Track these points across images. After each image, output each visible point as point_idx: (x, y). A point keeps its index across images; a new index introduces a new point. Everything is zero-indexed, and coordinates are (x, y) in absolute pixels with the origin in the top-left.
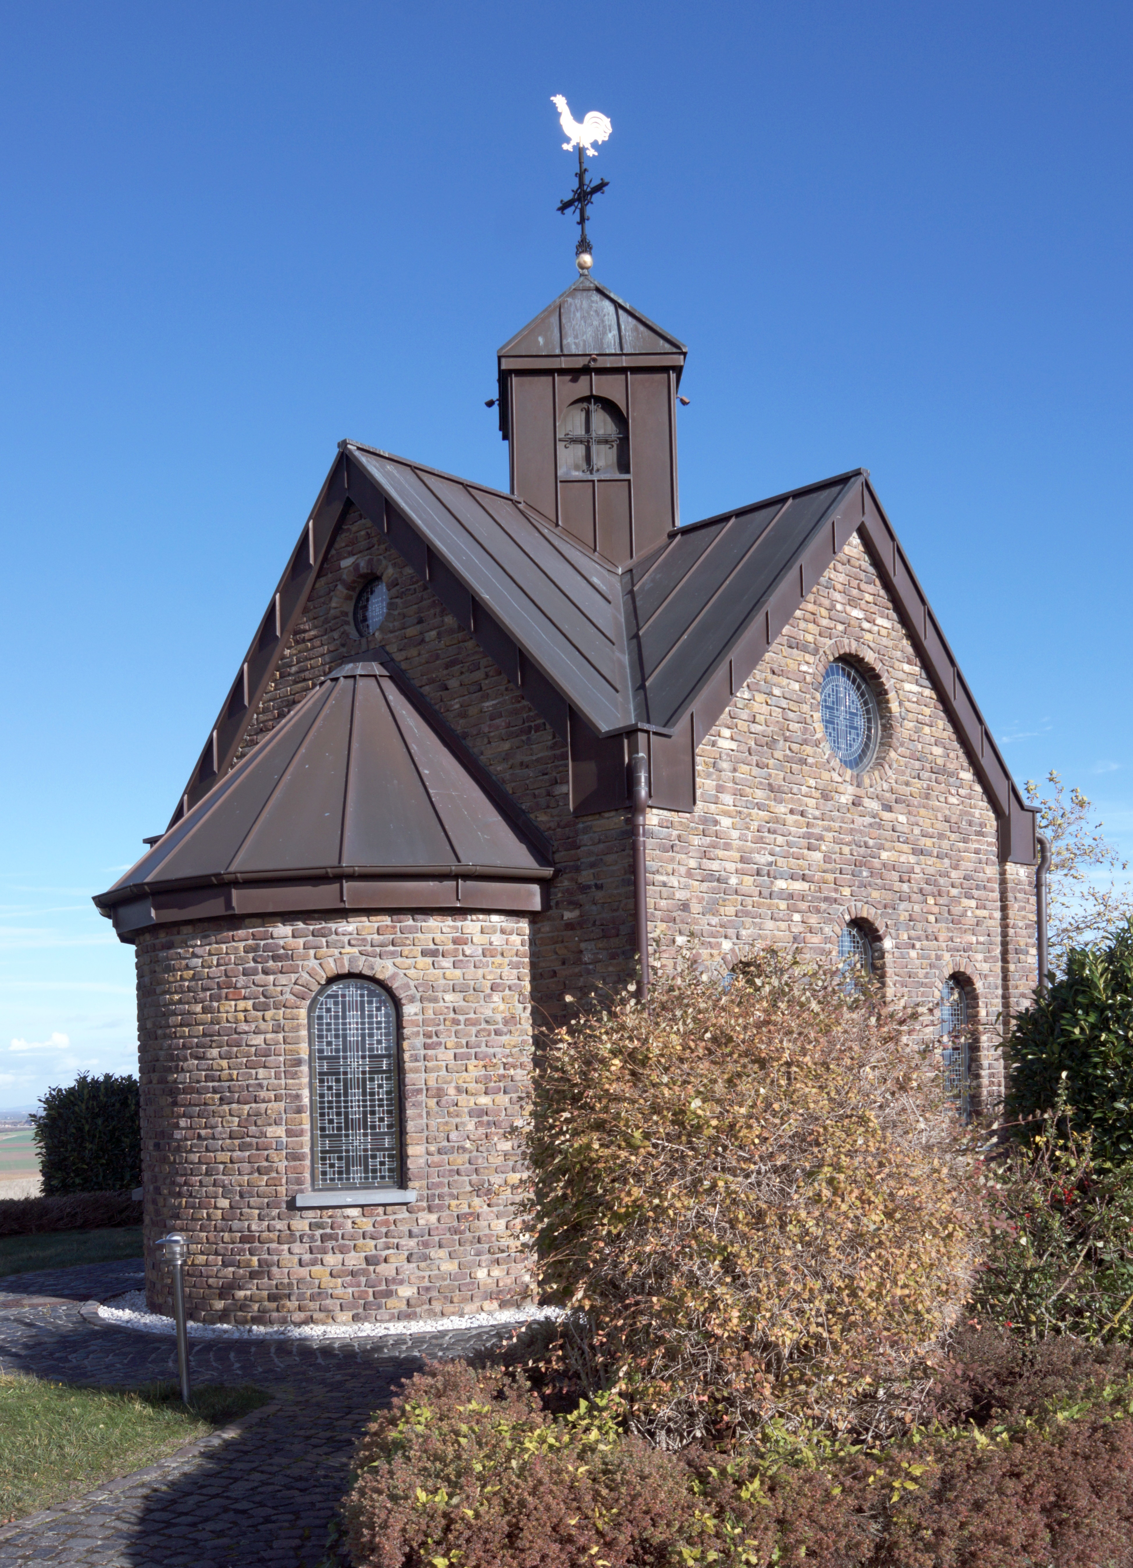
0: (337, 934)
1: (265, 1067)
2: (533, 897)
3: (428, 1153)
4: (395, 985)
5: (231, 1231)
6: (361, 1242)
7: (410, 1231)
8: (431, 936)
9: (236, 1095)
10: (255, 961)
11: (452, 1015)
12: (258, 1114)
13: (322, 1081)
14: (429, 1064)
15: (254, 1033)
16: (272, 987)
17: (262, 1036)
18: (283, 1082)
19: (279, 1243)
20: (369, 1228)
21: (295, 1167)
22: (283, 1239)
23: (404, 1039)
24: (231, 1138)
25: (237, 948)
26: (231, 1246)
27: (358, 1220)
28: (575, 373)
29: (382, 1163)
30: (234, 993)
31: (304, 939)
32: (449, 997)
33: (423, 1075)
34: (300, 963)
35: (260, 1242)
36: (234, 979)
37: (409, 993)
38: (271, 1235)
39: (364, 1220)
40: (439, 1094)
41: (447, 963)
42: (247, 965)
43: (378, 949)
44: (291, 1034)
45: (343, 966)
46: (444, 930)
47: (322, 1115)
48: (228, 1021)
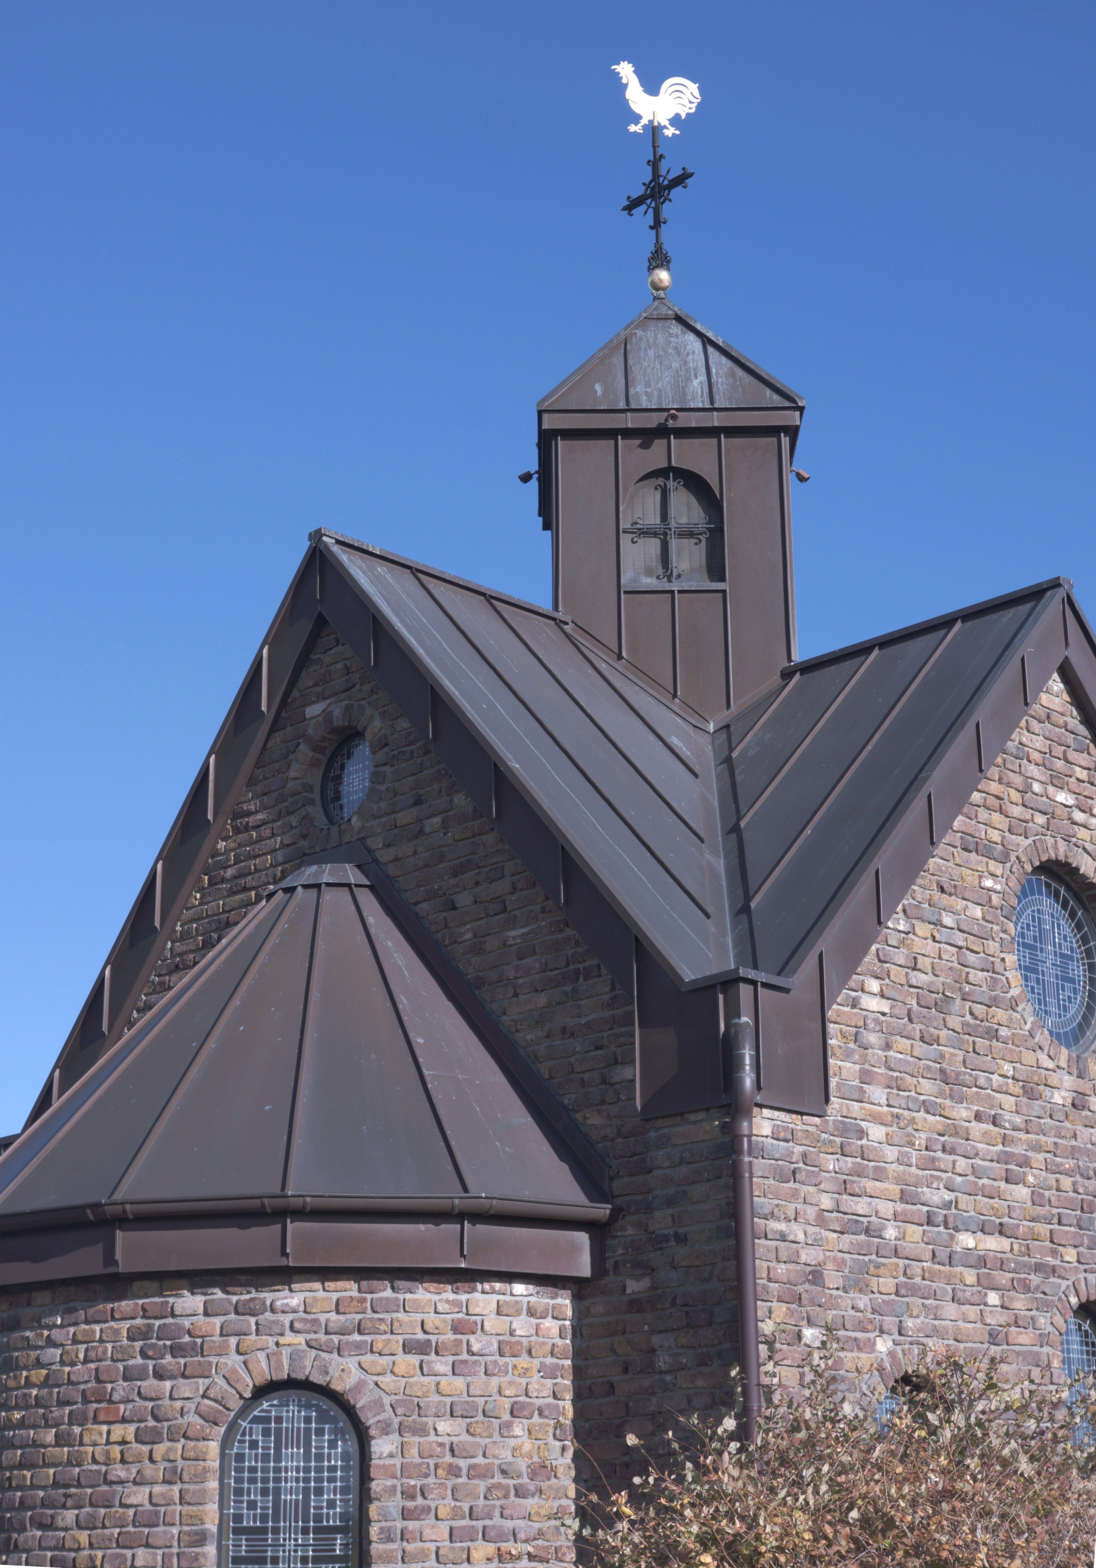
0: (273, 1310)
2: (578, 1254)
4: (360, 1402)
8: (419, 1317)
10: (144, 1355)
11: (448, 1459)
14: (410, 1547)
15: (135, 1483)
16: (167, 1402)
17: (147, 1490)
23: (370, 1500)
25: (117, 1332)
28: (646, 436)
31: (222, 1319)
32: (444, 1426)
36: (109, 1386)
37: (381, 1417)
41: (442, 1365)
42: (131, 1362)
43: (335, 1339)
44: (192, 1487)
45: (280, 1366)
46: (440, 1308)
48: (94, 1461)
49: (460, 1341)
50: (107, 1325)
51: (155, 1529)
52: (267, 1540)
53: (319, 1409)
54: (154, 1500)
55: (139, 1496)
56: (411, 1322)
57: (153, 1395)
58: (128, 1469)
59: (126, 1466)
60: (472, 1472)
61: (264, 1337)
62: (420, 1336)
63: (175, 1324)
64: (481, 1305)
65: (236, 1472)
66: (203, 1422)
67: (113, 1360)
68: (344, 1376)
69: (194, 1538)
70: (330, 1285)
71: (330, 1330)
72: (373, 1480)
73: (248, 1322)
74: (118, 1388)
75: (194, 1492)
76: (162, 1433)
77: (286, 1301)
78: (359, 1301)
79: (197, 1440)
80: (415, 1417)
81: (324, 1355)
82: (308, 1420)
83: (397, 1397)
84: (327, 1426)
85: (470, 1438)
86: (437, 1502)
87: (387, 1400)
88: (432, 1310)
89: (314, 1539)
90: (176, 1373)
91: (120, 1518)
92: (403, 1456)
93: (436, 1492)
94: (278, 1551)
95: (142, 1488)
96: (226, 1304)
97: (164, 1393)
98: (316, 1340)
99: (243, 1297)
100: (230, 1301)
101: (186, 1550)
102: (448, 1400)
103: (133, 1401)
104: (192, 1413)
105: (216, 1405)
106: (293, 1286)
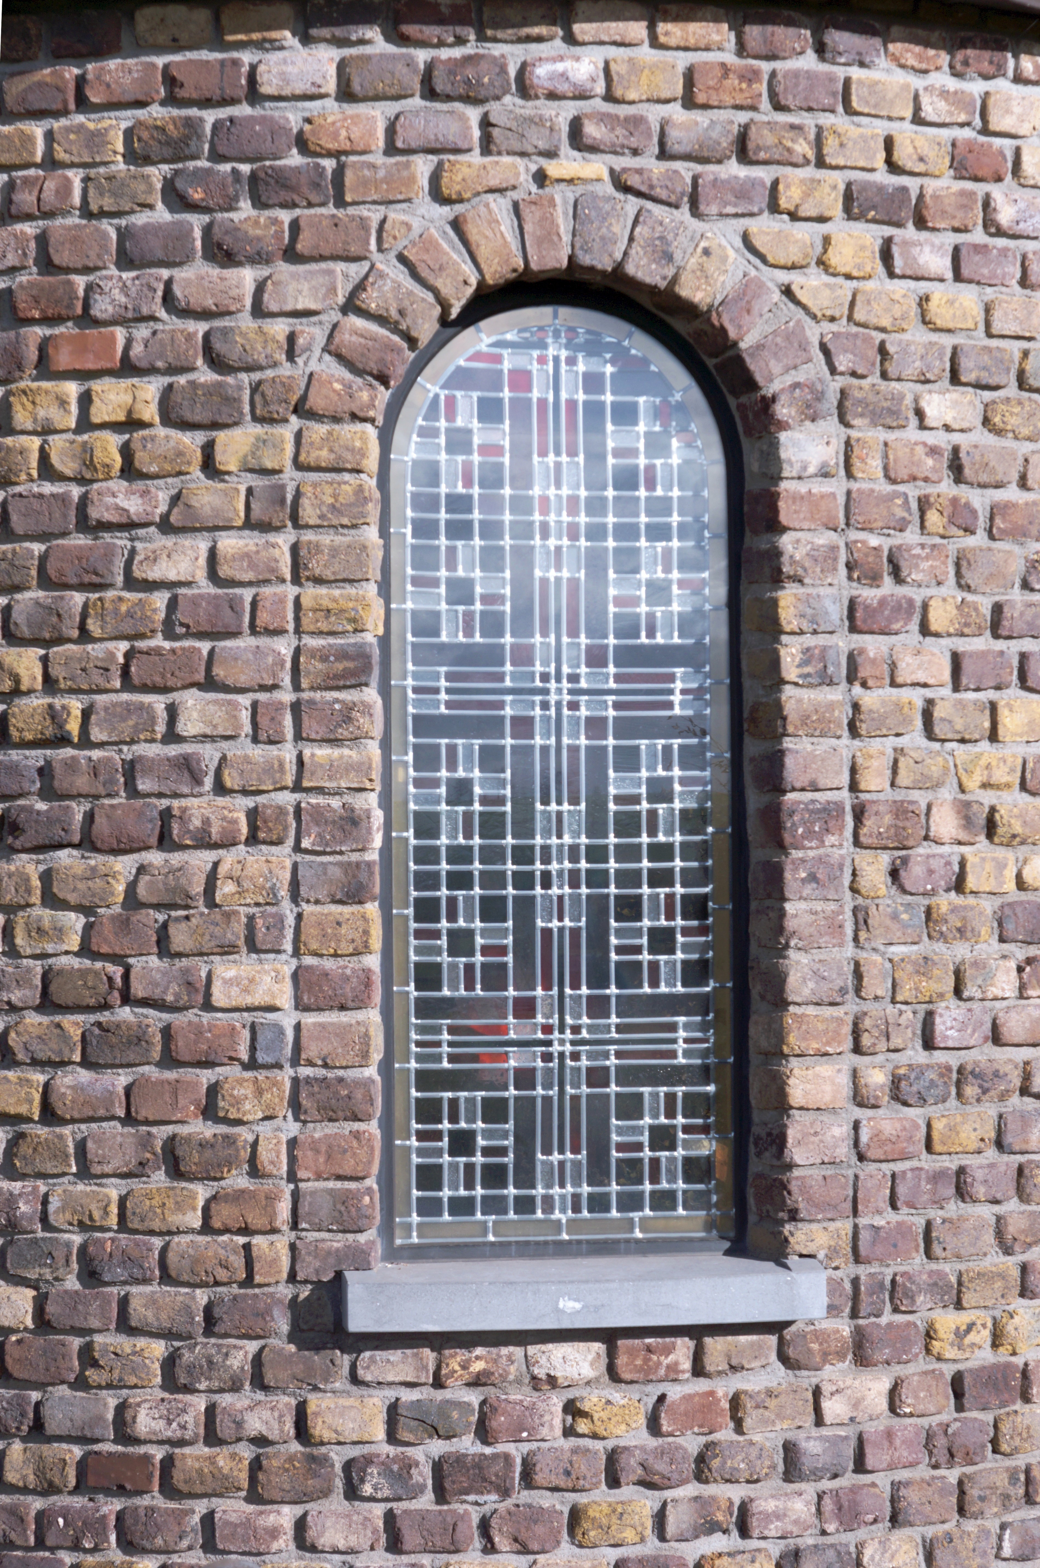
0: (524, 90)
1: (210, 684)
3: (859, 1099)
4: (749, 337)
5: (37, 1430)
6: (598, 1498)
7: (790, 1450)
8: (881, 128)
9: (78, 811)
10: (176, 198)
11: (946, 488)
12: (175, 901)
13: (426, 758)
14: (870, 699)
15: (166, 526)
16: (245, 322)
17: (202, 545)
18: (288, 753)
19: (254, 1497)
20: (633, 1435)
21: (331, 1150)
22: (275, 1479)
23: (777, 579)
24: (48, 1003)
25: (97, 140)
26: (37, 1504)
27: (591, 1401)
29: (663, 1138)
30: (81, 347)
31: (392, 108)
32: (941, 405)
33: (845, 744)
34: (374, 214)
35: (169, 1490)
36: (80, 282)
37: (800, 376)
38: (223, 1458)
39: (617, 1395)
40: (904, 834)
41: (931, 253)
42: (141, 219)
43: (686, 170)
44: (326, 539)
45: (550, 235)
46: (929, 112)
47: (427, 910)
48: (47, 470)
49: (972, 194)
50: (63, 122)
51: (228, 643)
52: (501, 677)
53: (620, 355)
54: (224, 571)
55: (181, 561)
56: (864, 138)
57: (209, 303)
58: (145, 493)
59: (140, 485)
60: (999, 522)
61: (506, 159)
62: (882, 177)
63: (263, 120)
64: (1017, 110)
65: (416, 507)
66: (348, 375)
67: (87, 213)
68: (711, 266)
69: (340, 666)
70: (671, 31)
71: (674, 147)
72: (784, 529)
73: (463, 119)
74: (106, 285)
75: (334, 551)
76: (238, 400)
77: (560, 67)
78: (742, 78)
79: (336, 419)
80: (875, 379)
81: (657, 210)
82: (593, 382)
83: (834, 327)
84: (642, 400)
85: (988, 439)
86: (929, 592)
87: (813, 333)
88: (908, 114)
89: (618, 678)
90: (271, 246)
91: (130, 614)
92: (850, 475)
93: (925, 565)
94: (532, 705)
95: (186, 541)
96: (401, 69)
97: (239, 299)
98: (639, 171)
99: (445, 54)
100: (410, 63)
101: (318, 695)
102: (948, 341)
103: (153, 318)
104: (317, 352)
105: (383, 332)
106: (577, 28)
